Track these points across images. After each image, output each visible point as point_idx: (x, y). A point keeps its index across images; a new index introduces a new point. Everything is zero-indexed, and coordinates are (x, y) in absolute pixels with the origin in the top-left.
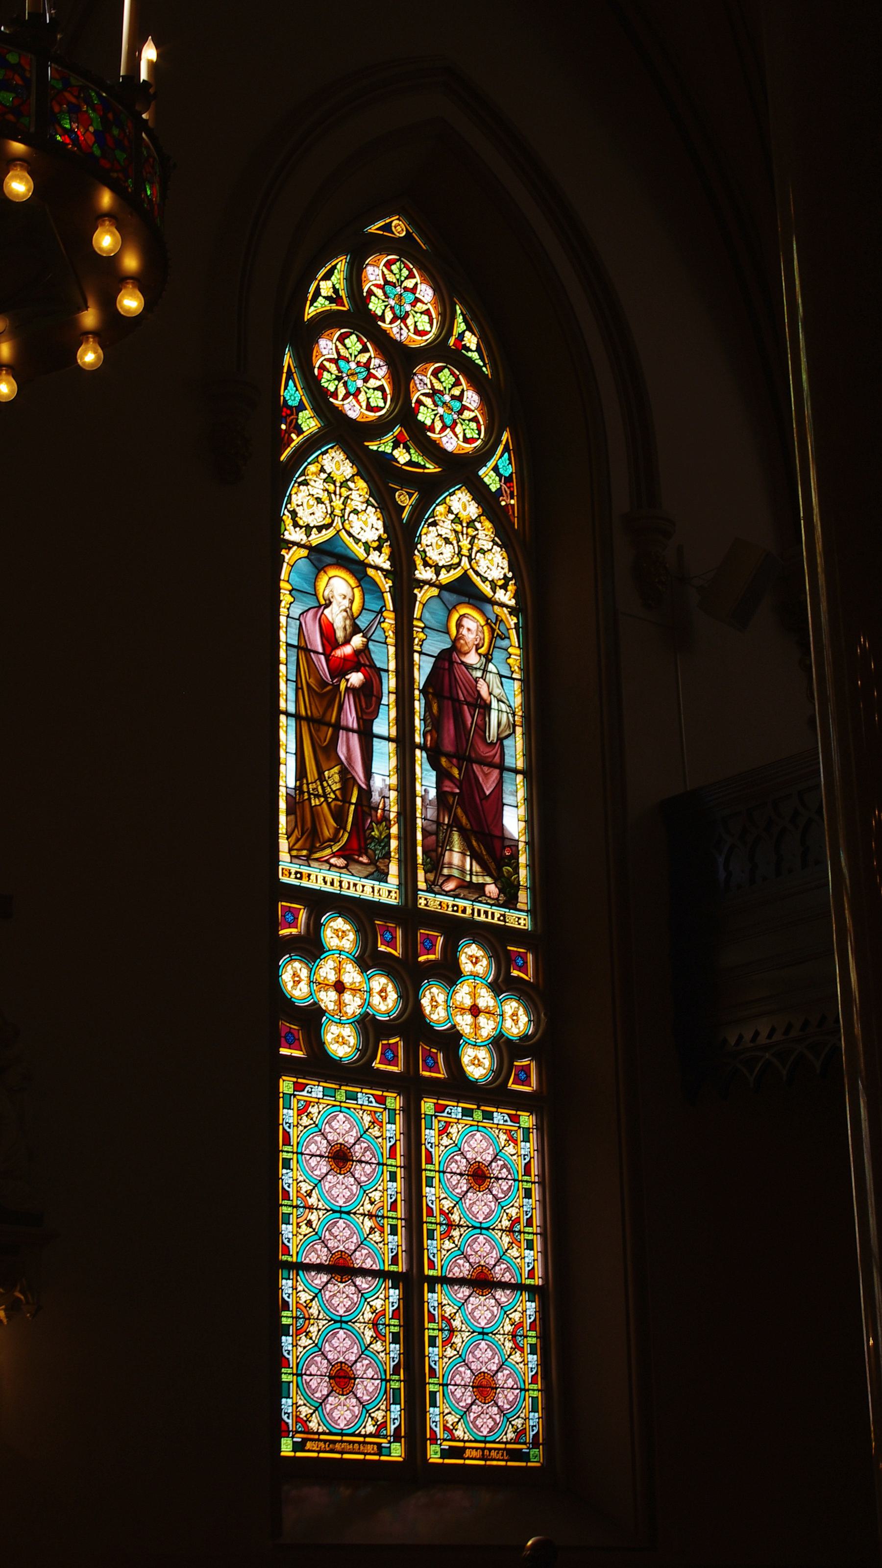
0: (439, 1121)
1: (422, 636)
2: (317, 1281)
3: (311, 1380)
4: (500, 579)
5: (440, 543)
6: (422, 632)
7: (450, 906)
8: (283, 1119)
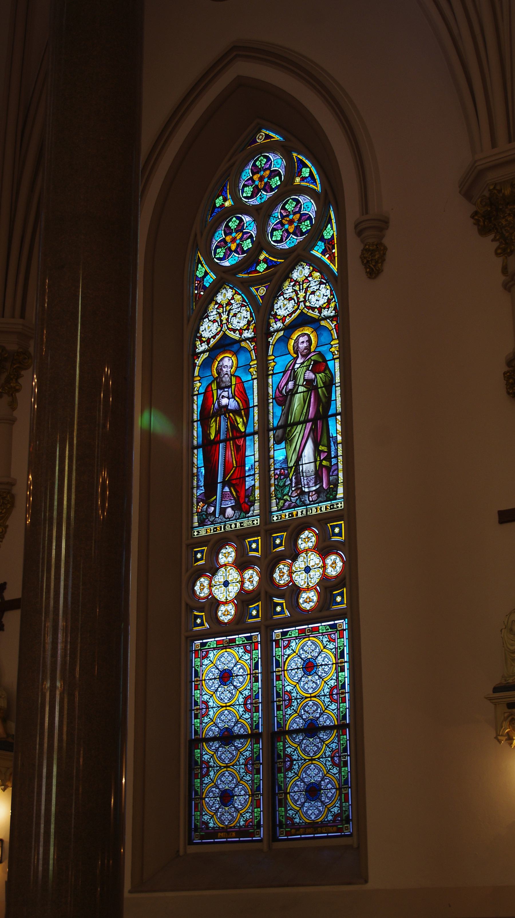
0: (203, 652)
1: (273, 364)
2: (297, 740)
3: (295, 795)
4: (325, 303)
5: (285, 303)
6: (274, 362)
7: (287, 515)
8: (275, 654)
